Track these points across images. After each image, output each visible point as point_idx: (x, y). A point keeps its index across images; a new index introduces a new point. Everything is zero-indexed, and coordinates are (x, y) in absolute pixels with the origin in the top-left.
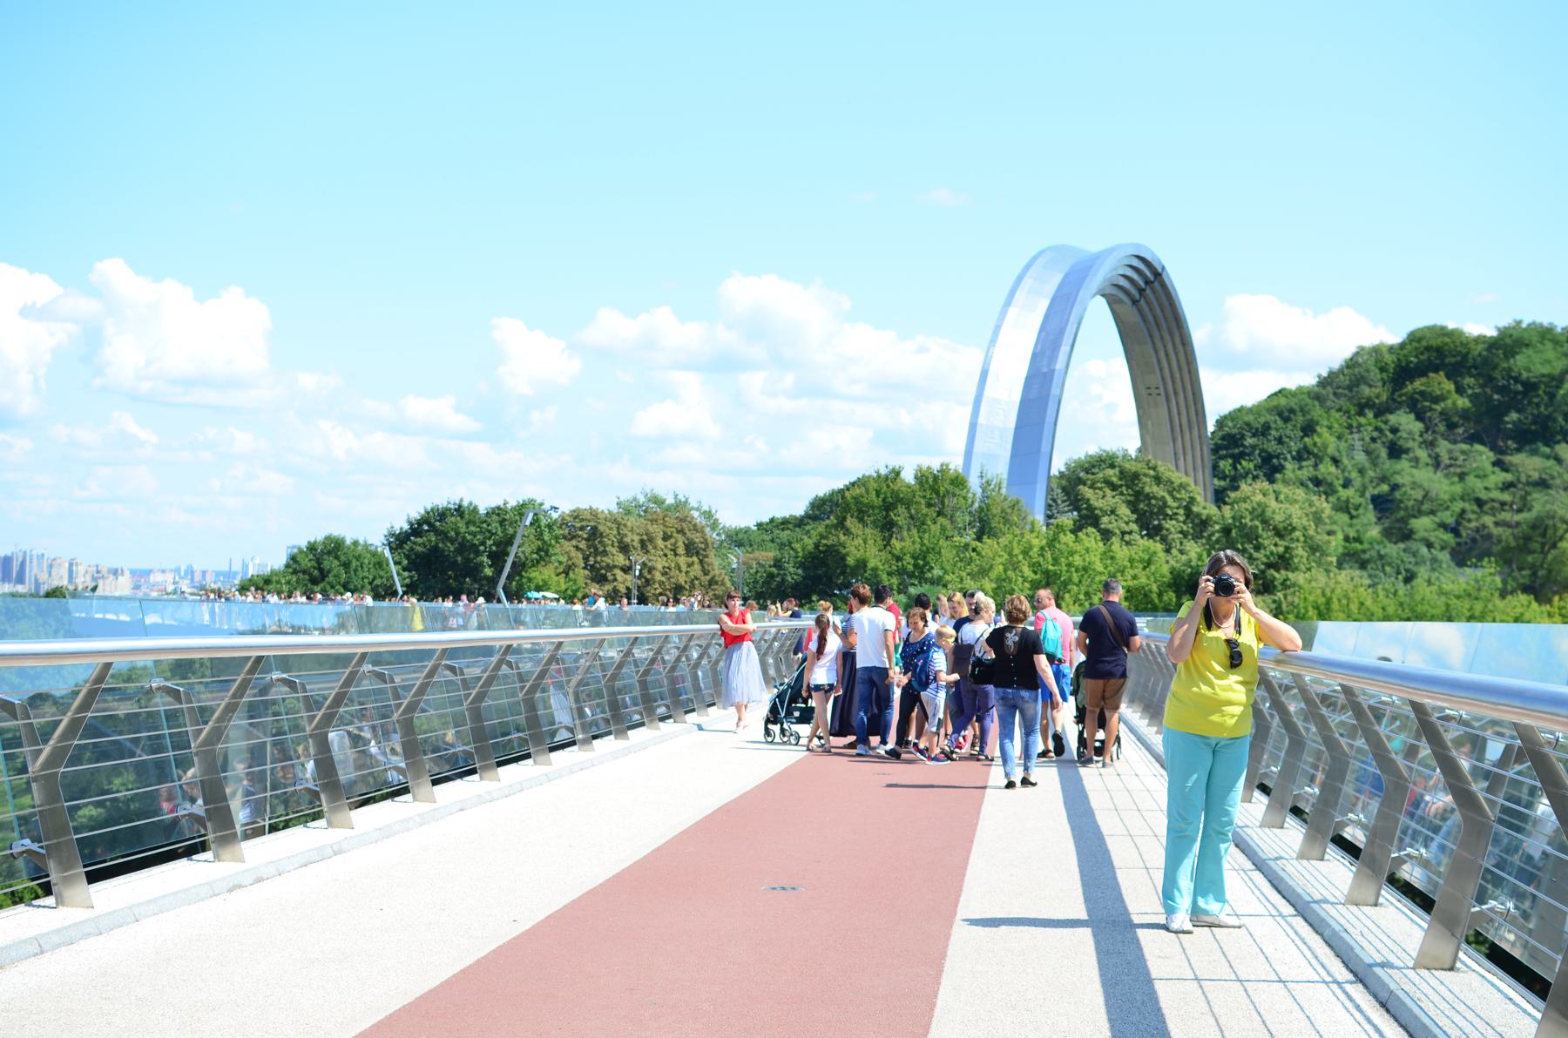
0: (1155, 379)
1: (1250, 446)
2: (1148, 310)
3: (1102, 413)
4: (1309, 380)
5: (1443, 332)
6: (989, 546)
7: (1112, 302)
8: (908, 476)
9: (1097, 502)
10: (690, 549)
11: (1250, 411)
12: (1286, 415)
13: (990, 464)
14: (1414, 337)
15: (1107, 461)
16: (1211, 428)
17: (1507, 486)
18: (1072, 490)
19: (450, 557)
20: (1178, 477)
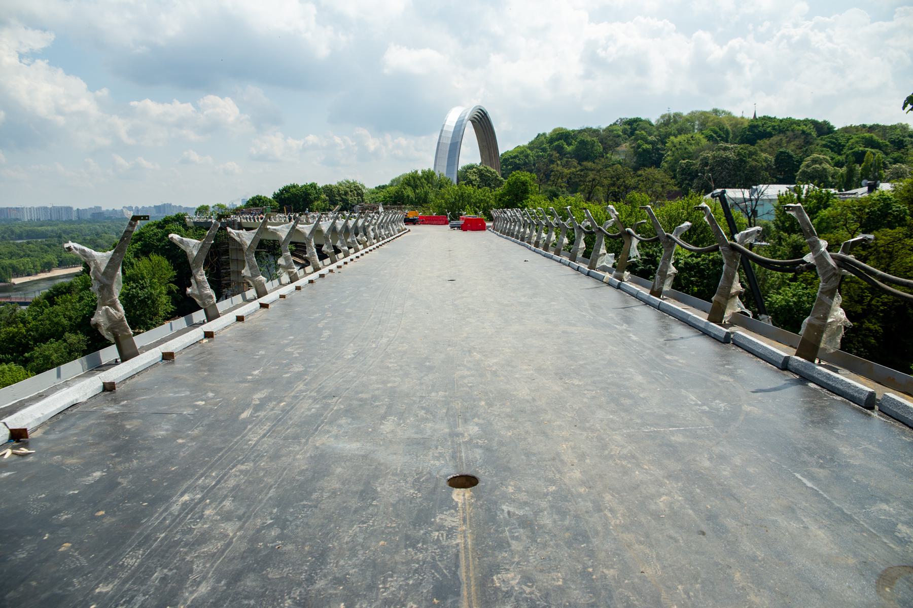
0: (485, 144)
1: (514, 162)
2: (482, 123)
3: (470, 154)
4: (526, 143)
5: (562, 129)
6: (443, 190)
7: (473, 122)
8: (420, 173)
9: (471, 177)
10: (358, 194)
11: (511, 152)
12: (522, 152)
13: (442, 171)
14: (555, 131)
15: (471, 167)
16: (460, 168)
17: (582, 170)
18: (463, 176)
19: (295, 201)
20: (493, 170)
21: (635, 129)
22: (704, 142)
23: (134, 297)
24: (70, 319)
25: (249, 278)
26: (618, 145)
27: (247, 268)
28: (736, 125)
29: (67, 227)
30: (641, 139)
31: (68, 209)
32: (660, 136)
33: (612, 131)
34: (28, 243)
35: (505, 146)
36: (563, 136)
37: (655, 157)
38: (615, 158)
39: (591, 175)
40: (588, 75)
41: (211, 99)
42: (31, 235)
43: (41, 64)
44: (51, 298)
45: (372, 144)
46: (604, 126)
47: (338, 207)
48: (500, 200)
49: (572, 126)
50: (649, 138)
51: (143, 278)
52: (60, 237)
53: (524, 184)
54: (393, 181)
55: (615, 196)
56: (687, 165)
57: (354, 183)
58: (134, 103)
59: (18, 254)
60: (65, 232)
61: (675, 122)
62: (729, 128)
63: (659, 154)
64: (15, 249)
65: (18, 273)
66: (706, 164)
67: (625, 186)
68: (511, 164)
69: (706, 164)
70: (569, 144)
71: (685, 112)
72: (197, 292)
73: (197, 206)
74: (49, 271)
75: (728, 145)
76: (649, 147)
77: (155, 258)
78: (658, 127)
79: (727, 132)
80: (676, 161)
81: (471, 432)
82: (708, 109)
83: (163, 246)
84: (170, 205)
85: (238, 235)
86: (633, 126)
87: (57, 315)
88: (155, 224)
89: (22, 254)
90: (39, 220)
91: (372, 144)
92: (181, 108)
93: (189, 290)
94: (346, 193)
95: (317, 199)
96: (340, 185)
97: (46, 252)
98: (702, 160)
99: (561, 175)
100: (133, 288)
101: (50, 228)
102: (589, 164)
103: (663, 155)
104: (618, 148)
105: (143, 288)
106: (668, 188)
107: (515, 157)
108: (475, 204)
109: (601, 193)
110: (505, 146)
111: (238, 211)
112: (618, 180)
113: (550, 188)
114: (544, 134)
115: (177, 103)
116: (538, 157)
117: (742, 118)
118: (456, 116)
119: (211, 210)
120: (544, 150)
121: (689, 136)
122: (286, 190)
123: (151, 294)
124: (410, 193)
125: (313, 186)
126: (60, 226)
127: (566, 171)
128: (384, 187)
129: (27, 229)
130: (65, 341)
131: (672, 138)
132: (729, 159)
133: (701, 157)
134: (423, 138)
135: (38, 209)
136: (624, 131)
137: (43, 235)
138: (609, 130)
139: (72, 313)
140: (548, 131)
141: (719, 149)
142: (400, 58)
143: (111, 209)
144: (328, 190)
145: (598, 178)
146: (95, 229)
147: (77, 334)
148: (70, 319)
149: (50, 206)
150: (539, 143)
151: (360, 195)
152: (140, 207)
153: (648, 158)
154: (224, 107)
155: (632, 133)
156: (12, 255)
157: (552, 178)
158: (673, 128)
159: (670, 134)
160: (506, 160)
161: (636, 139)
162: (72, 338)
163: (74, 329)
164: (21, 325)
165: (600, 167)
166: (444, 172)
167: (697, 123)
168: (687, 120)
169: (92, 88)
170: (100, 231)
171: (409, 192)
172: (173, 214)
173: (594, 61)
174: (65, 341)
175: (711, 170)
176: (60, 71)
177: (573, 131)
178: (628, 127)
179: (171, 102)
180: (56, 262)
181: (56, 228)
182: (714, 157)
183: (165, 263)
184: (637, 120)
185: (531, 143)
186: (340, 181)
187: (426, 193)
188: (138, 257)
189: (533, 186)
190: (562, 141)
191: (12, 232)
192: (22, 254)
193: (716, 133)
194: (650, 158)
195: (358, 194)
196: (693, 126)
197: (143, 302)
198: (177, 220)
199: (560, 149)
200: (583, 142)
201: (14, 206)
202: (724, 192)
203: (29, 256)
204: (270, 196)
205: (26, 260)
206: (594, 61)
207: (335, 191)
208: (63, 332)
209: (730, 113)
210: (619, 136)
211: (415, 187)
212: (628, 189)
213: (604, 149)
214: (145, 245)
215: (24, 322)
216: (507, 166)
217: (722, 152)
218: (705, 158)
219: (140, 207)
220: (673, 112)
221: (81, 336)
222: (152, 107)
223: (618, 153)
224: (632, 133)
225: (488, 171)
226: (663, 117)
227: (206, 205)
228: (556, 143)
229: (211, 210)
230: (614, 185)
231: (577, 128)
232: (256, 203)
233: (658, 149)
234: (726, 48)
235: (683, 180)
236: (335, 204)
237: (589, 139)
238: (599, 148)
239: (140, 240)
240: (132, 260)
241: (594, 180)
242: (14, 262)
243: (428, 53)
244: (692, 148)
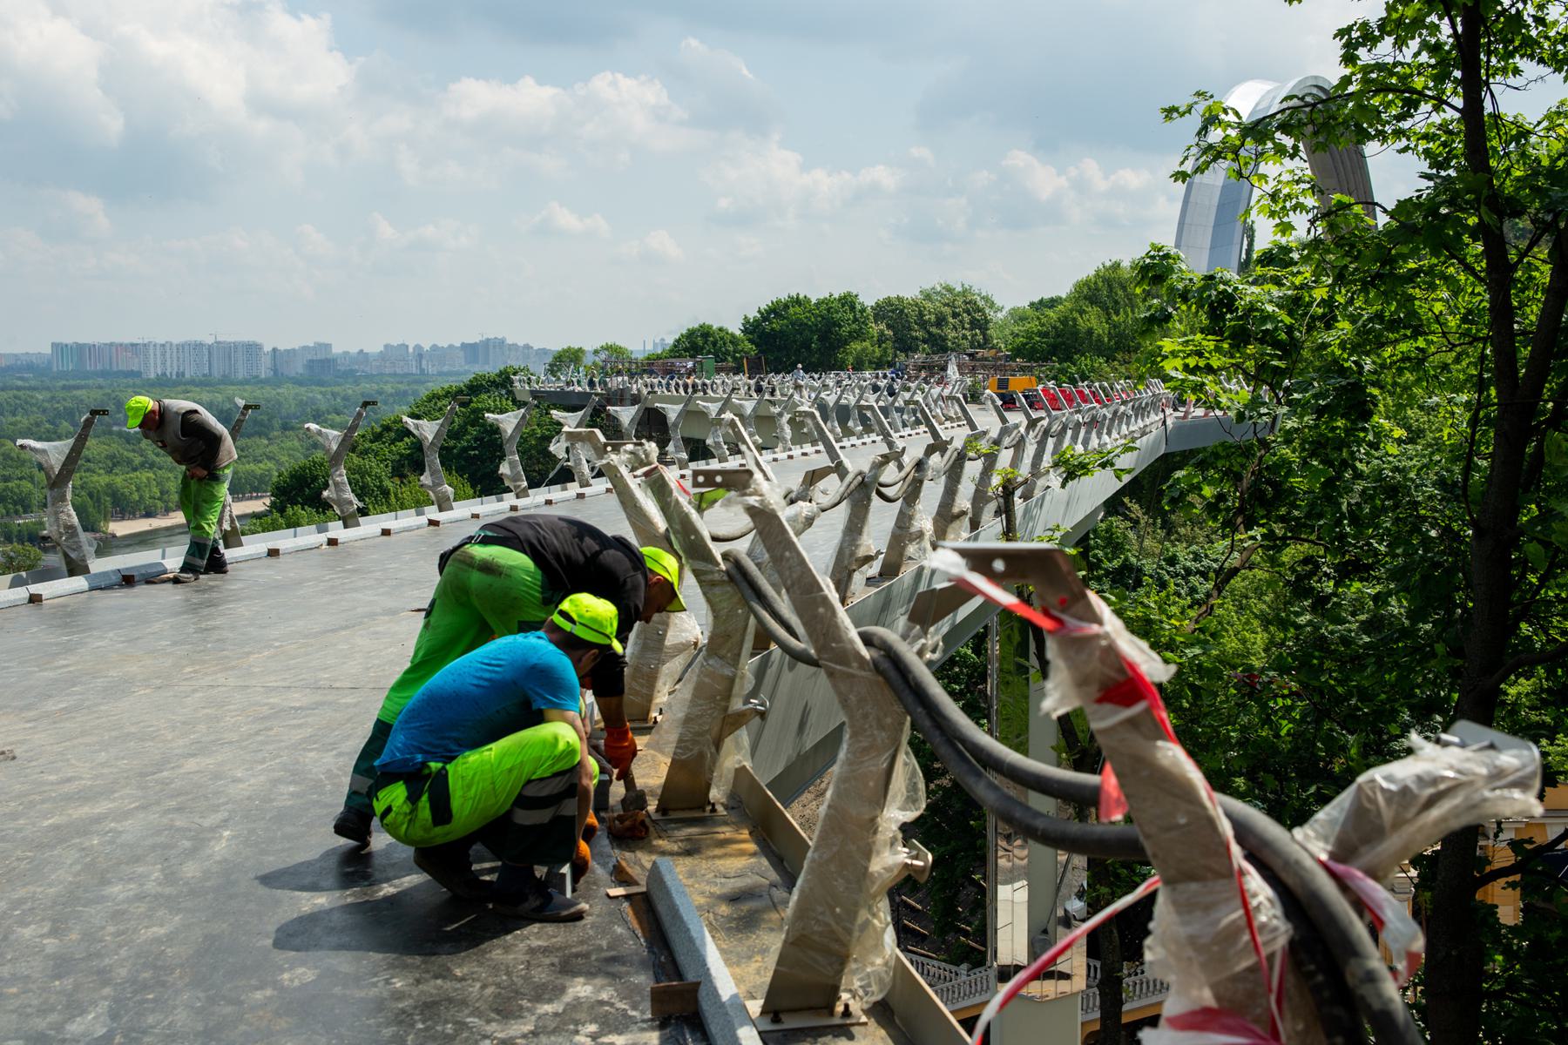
10: (975, 324)
19: (796, 339)
25: (430, 487)
27: (427, 473)
31: (252, 349)
45: (1045, 180)
57: (964, 292)
59: (129, 462)
65: (124, 509)
72: (334, 496)
73: (557, 345)
81: (1069, 908)
83: (465, 449)
84: (502, 341)
85: (417, 427)
88: (447, 394)
89: (138, 460)
90: (181, 374)
91: (1045, 180)
92: (531, 98)
93: (325, 493)
94: (940, 321)
95: (858, 335)
96: (928, 297)
111: (650, 366)
115: (528, 83)
119: (588, 360)
122: (776, 311)
124: (1094, 323)
125: (848, 302)
128: (1053, 303)
135: (181, 347)
143: (354, 350)
144: (891, 311)
146: (313, 401)
149: (210, 340)
151: (981, 324)
152: (427, 347)
170: (323, 407)
171: (1093, 321)
172: (491, 369)
186: (927, 287)
188: (402, 476)
192: (138, 460)
201: (127, 341)
203: (152, 466)
205: (145, 475)
207: (912, 313)
219: (427, 347)
229: (588, 360)
232: (700, 347)
240: (387, 483)
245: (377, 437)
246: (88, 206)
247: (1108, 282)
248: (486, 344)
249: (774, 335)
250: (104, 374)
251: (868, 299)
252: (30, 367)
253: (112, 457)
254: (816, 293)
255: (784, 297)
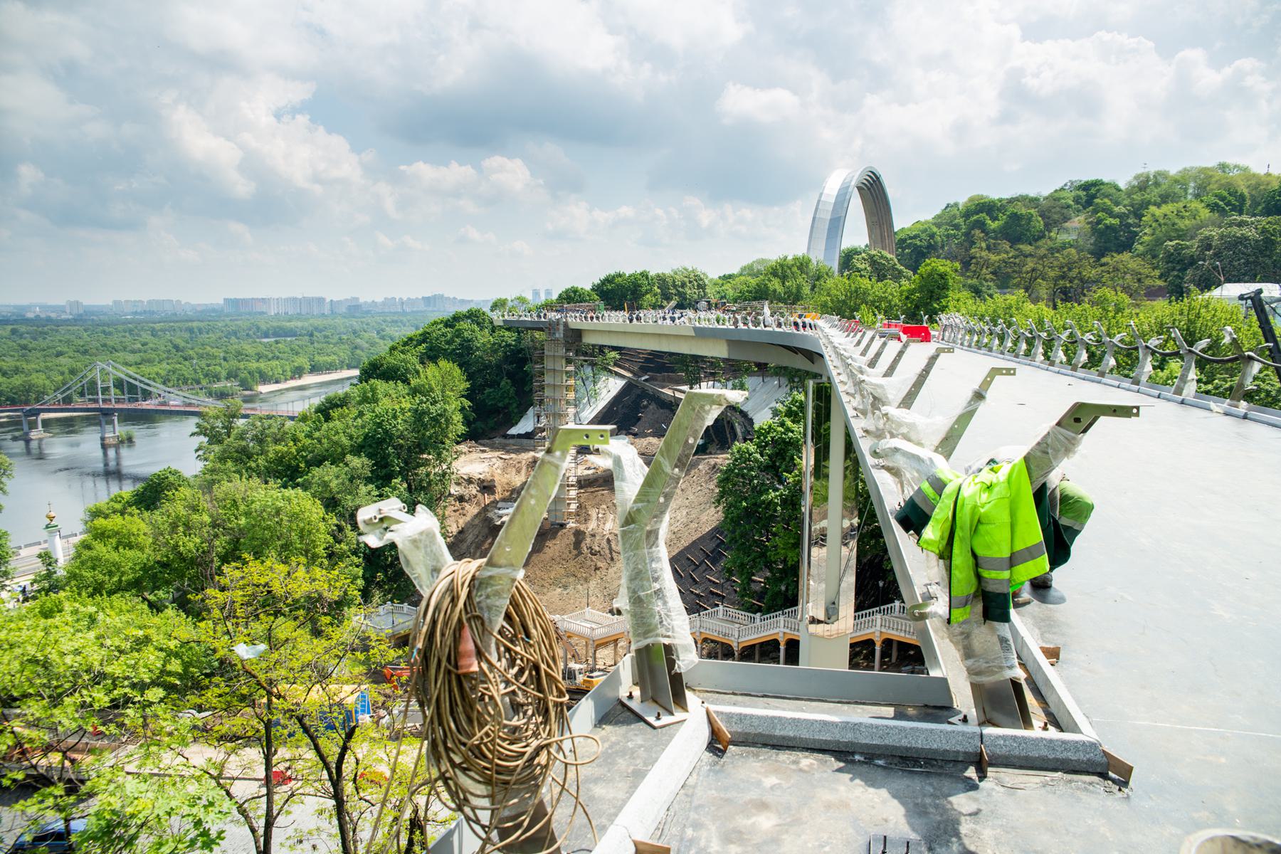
0: (875, 219)
2: (873, 193)
5: (982, 197)
7: (859, 189)
9: (859, 265)
10: (699, 286)
11: (910, 229)
12: (925, 230)
14: (971, 200)
18: (847, 260)
20: (889, 256)
21: (1094, 197)
22: (1205, 213)
23: (424, 413)
24: (351, 438)
26: (1066, 219)
28: (1256, 187)
29: (319, 322)
30: (1103, 210)
31: (321, 301)
32: (1132, 206)
33: (1059, 199)
34: (277, 342)
35: (904, 220)
36: (989, 208)
37: (1123, 236)
38: (1064, 237)
39: (1030, 264)
40: (1006, 118)
41: (496, 161)
42: (280, 333)
43: (302, 119)
44: (325, 411)
46: (1046, 193)
47: (673, 303)
48: (907, 298)
49: (997, 192)
50: (1116, 209)
51: (432, 390)
52: (311, 335)
53: (943, 276)
54: (743, 269)
55: (1065, 293)
56: (1176, 248)
58: (403, 168)
60: (316, 329)
61: (1157, 184)
62: (1246, 192)
63: (1131, 232)
64: (261, 349)
65: (265, 379)
66: (1209, 247)
67: (1081, 280)
68: (909, 246)
69: (1209, 247)
70: (994, 219)
71: (1173, 169)
74: (300, 377)
75: (1245, 218)
76: (1116, 221)
77: (443, 363)
78: (1129, 194)
79: (1242, 198)
80: (1159, 242)
82: (1211, 163)
86: (1090, 193)
87: (337, 433)
89: (271, 356)
92: (456, 173)
97: (297, 353)
98: (1201, 241)
99: (987, 264)
100: (422, 402)
101: (299, 324)
102: (1027, 248)
103: (1136, 234)
104: (1066, 225)
105: (434, 403)
106: (1148, 282)
107: (915, 237)
108: (873, 302)
109: (1043, 289)
110: (904, 220)
112: (1070, 270)
113: (970, 281)
114: (956, 205)
115: (454, 165)
116: (948, 236)
117: (1268, 175)
118: (840, 178)
120: (957, 227)
121: (1181, 205)
123: (445, 410)
125: (644, 275)
126: (311, 321)
127: (993, 258)
128: (730, 276)
129: (275, 324)
130: (347, 465)
131: (1152, 208)
132: (1247, 239)
133: (1200, 237)
134: (776, 209)
136: (1077, 200)
137: (292, 333)
138: (1054, 198)
139: (353, 431)
140: (962, 199)
141: (1230, 225)
142: (742, 102)
143: (369, 300)
144: (662, 280)
145: (1040, 267)
146: (352, 326)
147: (360, 456)
148: (351, 438)
149: (300, 296)
150: (948, 218)
151: (702, 287)
153: (1112, 239)
154: (510, 172)
155: (1089, 202)
156: (259, 357)
157: (973, 267)
158: (1153, 194)
159: (1149, 203)
160: (903, 241)
161: (1095, 212)
162: (356, 462)
163: (357, 451)
164: (291, 443)
165: (1042, 251)
166: (821, 257)
167: (1192, 185)
168: (1176, 181)
169: (356, 148)
170: (358, 328)
171: (775, 285)
172: (464, 309)
173: (1018, 97)
174: (347, 465)
175: (1217, 255)
176: (321, 128)
177: (1000, 200)
178: (1082, 193)
179: (447, 165)
180: (308, 367)
181: (306, 324)
182: (1222, 237)
183: (457, 371)
184: (1095, 184)
185: (939, 217)
187: (799, 287)
189: (954, 279)
190: (984, 215)
191: (258, 328)
193: (1223, 199)
194: (1116, 238)
195: (699, 286)
196: (1185, 190)
197: (435, 420)
198: (468, 317)
199: (981, 225)
200: (1015, 217)
202: (1260, 291)
204: (588, 287)
205: (274, 363)
206: (1018, 97)
208: (344, 455)
209: (1246, 169)
210: (1069, 206)
211: (784, 278)
212: (1086, 284)
213: (1046, 225)
214: (430, 349)
215: (295, 440)
216: (904, 249)
217: (1235, 229)
218: (1207, 238)
220: (1152, 169)
221: (365, 460)
222: (424, 171)
223: (1067, 230)
224: (1089, 202)
225: (882, 257)
226: (1136, 178)
227: (504, 297)
228: (975, 217)
229: (510, 304)
230: (1063, 277)
231: (1006, 195)
232: (572, 297)
233: (1128, 225)
234: (1228, 71)
235: (1169, 271)
236: (668, 299)
237: (1024, 211)
238: (1039, 223)
239: (424, 341)
241: (1033, 270)
242: (262, 365)
243: (783, 97)
244: (1184, 224)
245: (405, 344)
246: (236, 227)
247: (782, 266)
248: (435, 297)
249: (609, 291)
250: (250, 314)
251: (652, 273)
252: (214, 310)
253: (258, 354)
254: (628, 270)
255: (613, 273)
